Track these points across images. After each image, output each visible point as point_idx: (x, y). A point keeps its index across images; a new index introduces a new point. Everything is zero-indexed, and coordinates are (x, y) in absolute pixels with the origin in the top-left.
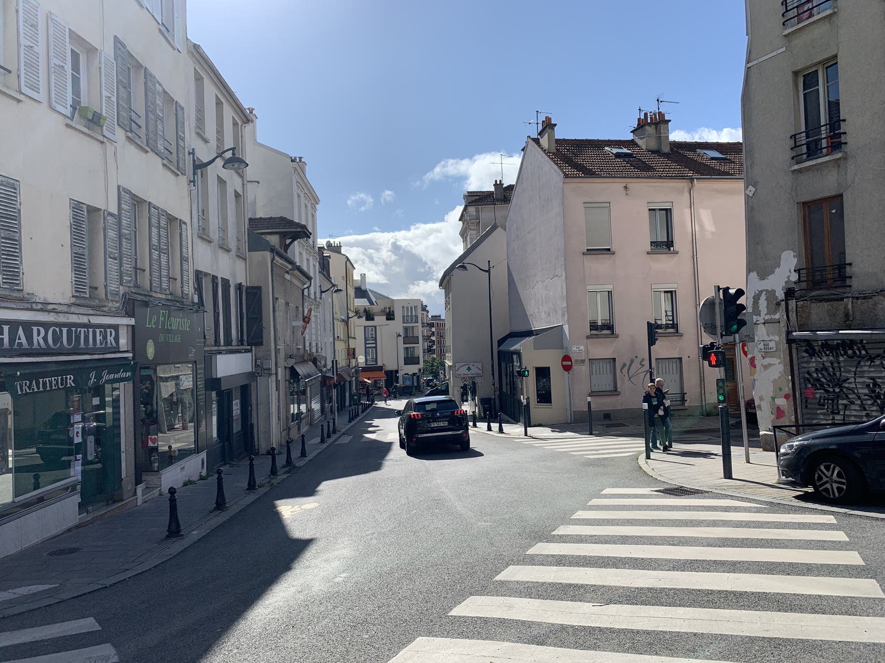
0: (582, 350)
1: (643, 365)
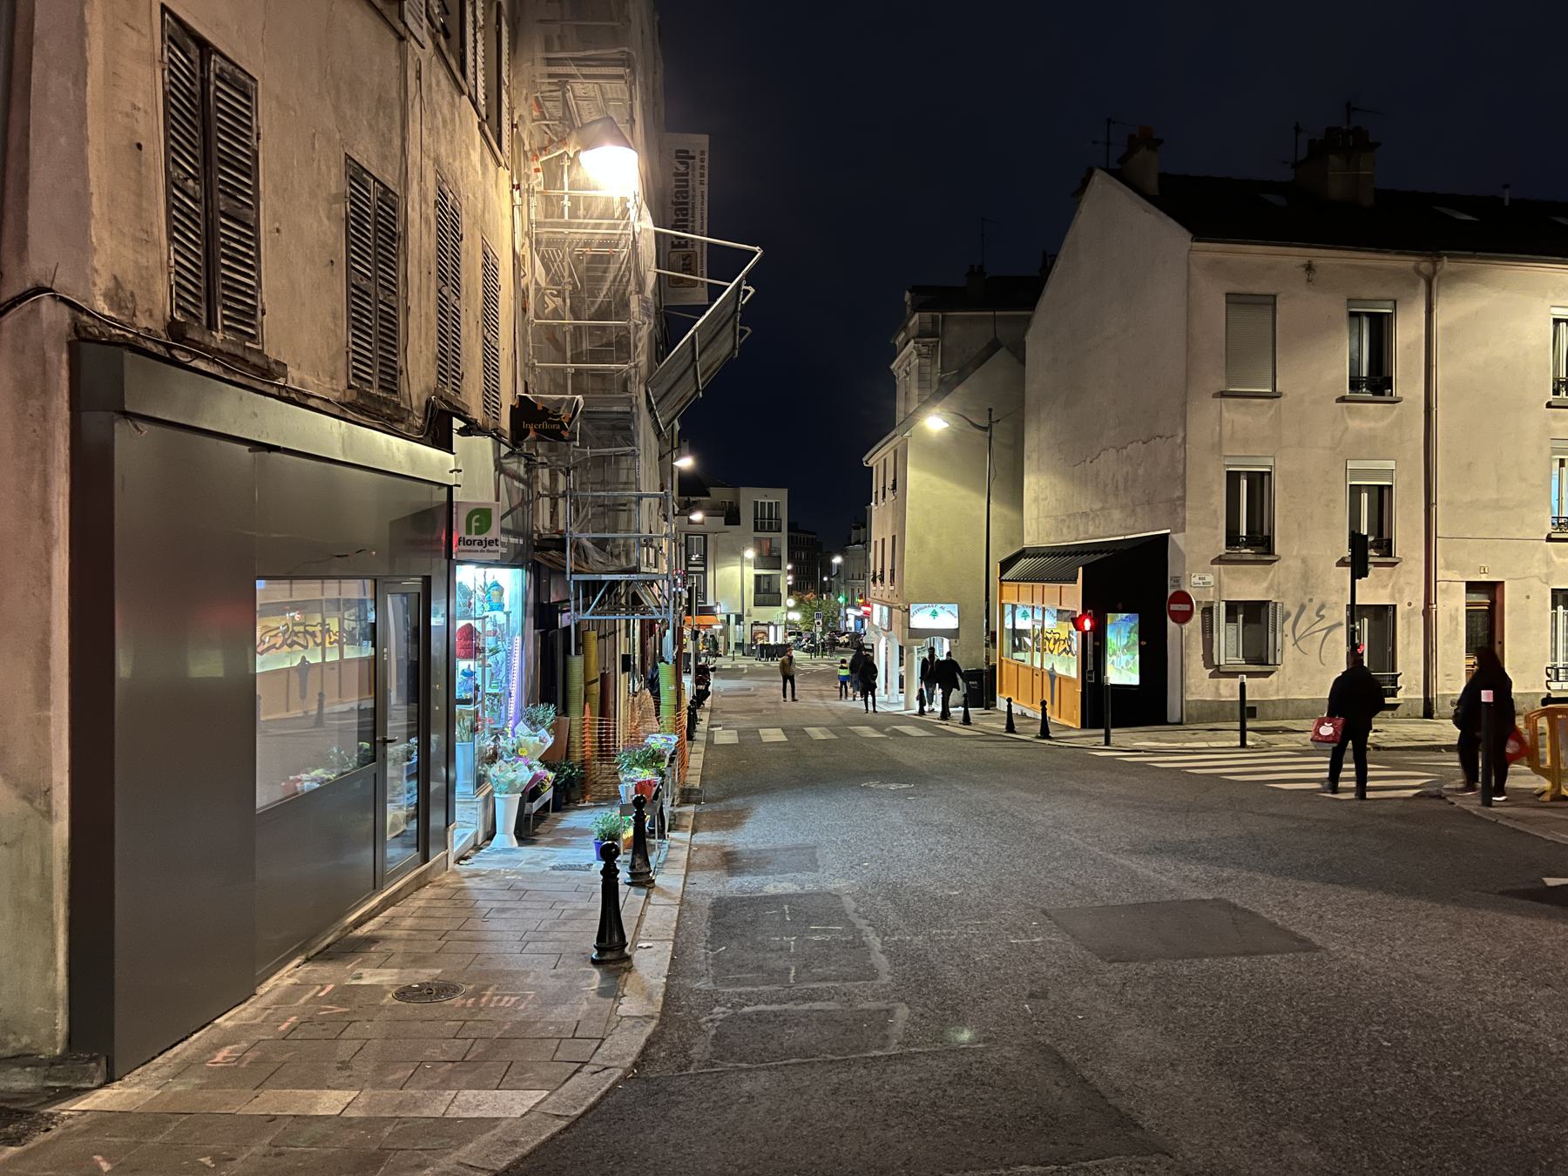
0: (1209, 583)
1: (1323, 617)
